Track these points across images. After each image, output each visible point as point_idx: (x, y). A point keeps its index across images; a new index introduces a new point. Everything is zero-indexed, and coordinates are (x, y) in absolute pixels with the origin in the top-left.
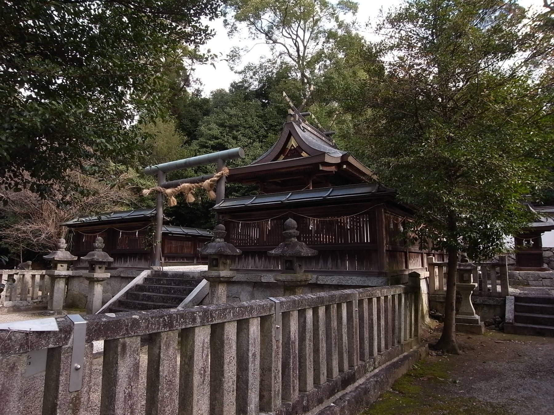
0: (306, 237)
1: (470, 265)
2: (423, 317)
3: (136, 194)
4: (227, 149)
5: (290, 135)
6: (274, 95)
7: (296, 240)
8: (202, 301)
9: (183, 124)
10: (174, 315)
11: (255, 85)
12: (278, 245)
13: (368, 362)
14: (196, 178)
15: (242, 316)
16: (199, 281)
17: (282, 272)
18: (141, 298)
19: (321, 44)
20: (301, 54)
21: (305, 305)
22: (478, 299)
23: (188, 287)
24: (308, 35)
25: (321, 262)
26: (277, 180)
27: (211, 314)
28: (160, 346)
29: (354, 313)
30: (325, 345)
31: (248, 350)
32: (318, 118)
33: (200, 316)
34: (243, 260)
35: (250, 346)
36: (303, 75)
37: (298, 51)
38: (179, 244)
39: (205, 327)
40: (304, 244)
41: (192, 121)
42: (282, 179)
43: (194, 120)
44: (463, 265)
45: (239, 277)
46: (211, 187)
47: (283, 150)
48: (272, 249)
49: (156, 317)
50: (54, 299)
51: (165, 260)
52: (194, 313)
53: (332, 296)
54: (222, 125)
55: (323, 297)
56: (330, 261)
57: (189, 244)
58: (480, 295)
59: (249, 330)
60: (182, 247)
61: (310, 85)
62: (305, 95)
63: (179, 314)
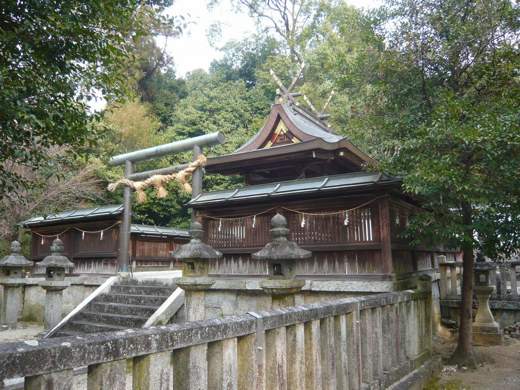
0: (297, 236)
1: (487, 264)
2: (434, 326)
3: (103, 189)
4: (204, 133)
5: (279, 118)
6: (259, 73)
7: (286, 239)
8: (176, 313)
9: (157, 109)
10: (121, 340)
11: (237, 65)
12: (264, 246)
13: (373, 384)
14: (171, 168)
15: (214, 338)
16: (172, 290)
17: (270, 277)
18: (106, 309)
19: (312, 17)
20: (291, 29)
21: (295, 320)
22: (496, 304)
23: (161, 296)
24: (297, 8)
25: (316, 264)
26: (266, 171)
27: (171, 337)
28: (102, 382)
29: (354, 326)
30: (320, 367)
31: (222, 379)
32: (311, 100)
33: (156, 340)
34: (225, 264)
35: (225, 374)
36: (293, 51)
37: (287, 25)
38: (153, 245)
39: (164, 354)
40: (295, 243)
41: (167, 105)
42: (270, 169)
43: (169, 105)
44: (479, 265)
45: (219, 284)
46: (186, 179)
47: (271, 136)
48: (257, 251)
49: (95, 344)
50: (7, 311)
51: (137, 264)
52: (147, 336)
53: (328, 307)
54: (202, 109)
55: (317, 309)
56: (326, 263)
57: (165, 245)
58: (499, 299)
59: (222, 355)
60: (156, 250)
61: (301, 63)
62: (295, 73)
63: (127, 339)
